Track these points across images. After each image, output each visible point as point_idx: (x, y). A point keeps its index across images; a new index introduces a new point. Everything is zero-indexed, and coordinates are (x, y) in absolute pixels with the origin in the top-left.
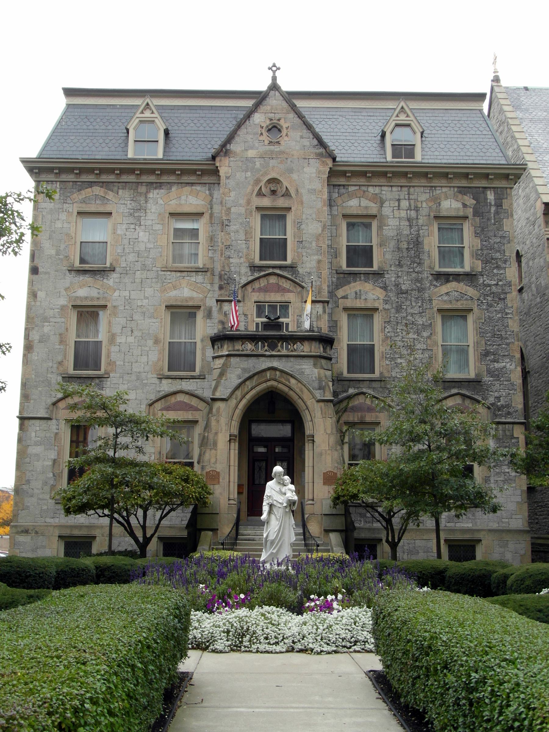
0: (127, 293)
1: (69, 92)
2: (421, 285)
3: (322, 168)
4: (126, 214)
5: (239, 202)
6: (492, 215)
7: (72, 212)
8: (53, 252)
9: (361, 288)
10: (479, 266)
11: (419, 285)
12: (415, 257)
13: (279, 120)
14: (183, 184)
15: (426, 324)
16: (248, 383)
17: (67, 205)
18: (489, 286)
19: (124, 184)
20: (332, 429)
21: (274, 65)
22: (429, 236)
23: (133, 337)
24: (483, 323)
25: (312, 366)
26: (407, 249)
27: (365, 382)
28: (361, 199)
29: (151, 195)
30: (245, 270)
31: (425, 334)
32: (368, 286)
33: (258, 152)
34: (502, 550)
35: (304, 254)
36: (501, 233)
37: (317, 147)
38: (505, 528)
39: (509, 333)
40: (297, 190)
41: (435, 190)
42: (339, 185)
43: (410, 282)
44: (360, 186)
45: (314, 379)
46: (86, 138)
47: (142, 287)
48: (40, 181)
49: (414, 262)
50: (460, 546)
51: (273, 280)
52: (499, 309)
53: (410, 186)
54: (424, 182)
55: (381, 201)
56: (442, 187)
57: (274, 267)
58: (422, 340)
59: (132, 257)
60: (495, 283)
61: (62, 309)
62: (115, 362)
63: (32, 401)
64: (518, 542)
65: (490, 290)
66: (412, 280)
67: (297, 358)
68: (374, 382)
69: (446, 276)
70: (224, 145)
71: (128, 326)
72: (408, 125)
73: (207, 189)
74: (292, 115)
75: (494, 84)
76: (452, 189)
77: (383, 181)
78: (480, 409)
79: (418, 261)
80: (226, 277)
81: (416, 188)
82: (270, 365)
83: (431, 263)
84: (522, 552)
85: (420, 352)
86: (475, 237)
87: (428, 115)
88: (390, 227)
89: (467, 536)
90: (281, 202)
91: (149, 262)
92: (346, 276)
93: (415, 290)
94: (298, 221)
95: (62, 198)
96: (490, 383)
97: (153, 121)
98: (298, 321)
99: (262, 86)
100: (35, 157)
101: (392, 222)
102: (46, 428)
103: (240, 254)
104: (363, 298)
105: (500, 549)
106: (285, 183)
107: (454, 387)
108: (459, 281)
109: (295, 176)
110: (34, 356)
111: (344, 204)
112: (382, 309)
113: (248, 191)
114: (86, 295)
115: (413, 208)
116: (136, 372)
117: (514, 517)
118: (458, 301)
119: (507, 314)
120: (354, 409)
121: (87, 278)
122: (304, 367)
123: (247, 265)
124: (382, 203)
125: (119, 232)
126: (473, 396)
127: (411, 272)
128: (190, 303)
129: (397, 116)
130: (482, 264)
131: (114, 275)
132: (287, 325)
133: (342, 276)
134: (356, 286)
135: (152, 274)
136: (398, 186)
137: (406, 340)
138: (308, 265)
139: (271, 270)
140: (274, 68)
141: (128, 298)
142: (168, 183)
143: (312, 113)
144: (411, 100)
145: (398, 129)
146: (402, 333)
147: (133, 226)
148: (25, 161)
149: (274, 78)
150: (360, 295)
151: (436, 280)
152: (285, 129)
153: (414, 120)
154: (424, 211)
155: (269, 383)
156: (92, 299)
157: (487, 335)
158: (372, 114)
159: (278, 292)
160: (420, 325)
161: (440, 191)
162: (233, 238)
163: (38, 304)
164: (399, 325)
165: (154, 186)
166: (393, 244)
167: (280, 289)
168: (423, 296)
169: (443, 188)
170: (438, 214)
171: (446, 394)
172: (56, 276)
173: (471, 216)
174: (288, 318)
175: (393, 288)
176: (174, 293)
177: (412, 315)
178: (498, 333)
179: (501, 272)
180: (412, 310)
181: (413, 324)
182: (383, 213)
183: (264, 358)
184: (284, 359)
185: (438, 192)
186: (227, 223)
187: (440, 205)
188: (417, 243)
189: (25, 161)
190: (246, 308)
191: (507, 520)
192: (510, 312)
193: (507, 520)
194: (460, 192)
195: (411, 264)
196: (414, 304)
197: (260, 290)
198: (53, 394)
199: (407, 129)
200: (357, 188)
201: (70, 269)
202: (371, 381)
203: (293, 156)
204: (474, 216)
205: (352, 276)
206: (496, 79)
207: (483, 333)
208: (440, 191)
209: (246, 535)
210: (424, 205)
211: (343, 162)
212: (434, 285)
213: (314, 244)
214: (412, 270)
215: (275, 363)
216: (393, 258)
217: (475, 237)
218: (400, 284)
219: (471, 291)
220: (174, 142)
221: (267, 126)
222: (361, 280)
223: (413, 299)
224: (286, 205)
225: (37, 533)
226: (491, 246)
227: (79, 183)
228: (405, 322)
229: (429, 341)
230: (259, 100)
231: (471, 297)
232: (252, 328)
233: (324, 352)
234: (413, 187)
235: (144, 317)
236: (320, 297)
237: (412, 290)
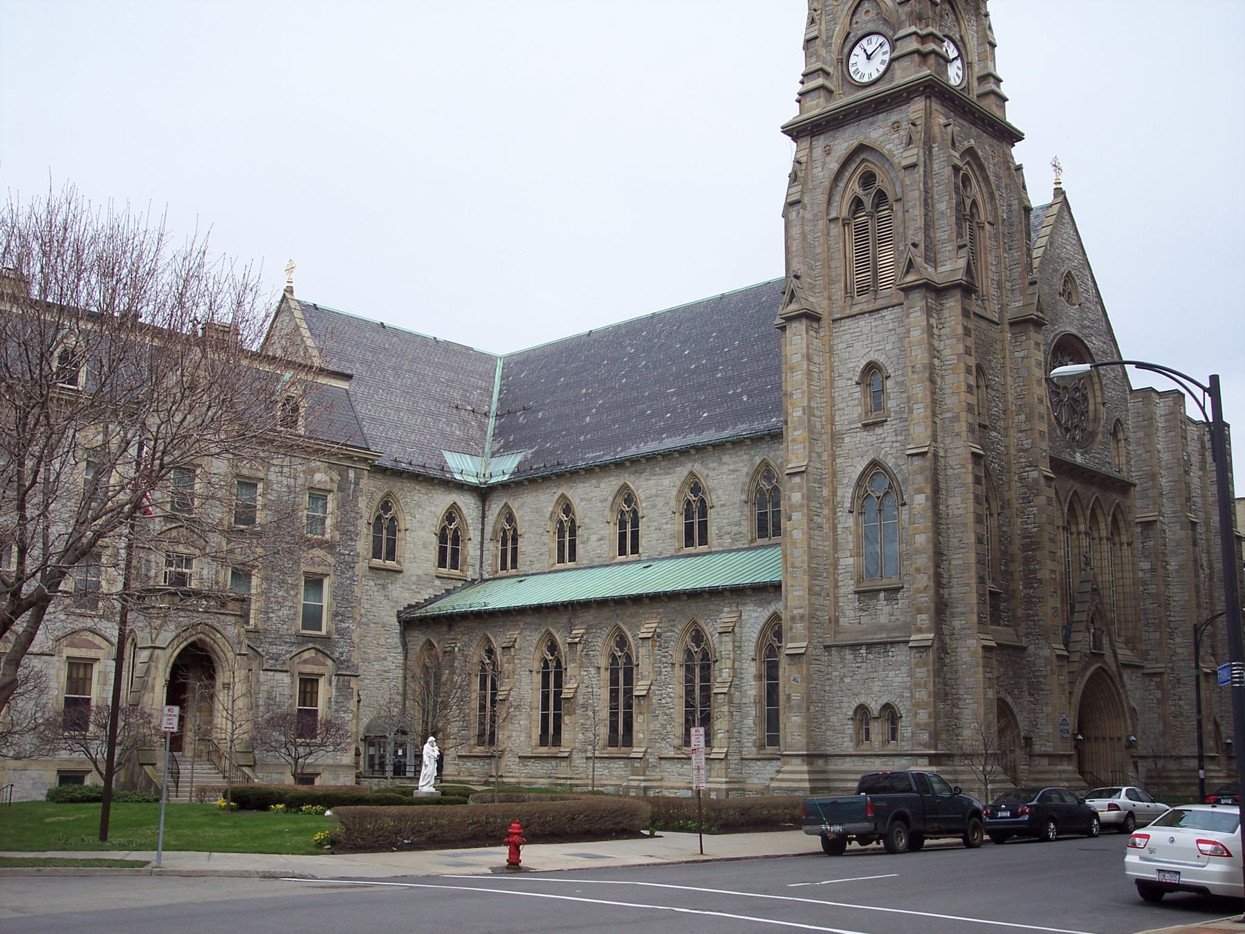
18: (344, 555)
85: (287, 608)
107: (310, 642)
119: (354, 581)
155: (201, 636)
179: (354, 543)
194: (329, 467)
206: (290, 290)
219: (330, 559)
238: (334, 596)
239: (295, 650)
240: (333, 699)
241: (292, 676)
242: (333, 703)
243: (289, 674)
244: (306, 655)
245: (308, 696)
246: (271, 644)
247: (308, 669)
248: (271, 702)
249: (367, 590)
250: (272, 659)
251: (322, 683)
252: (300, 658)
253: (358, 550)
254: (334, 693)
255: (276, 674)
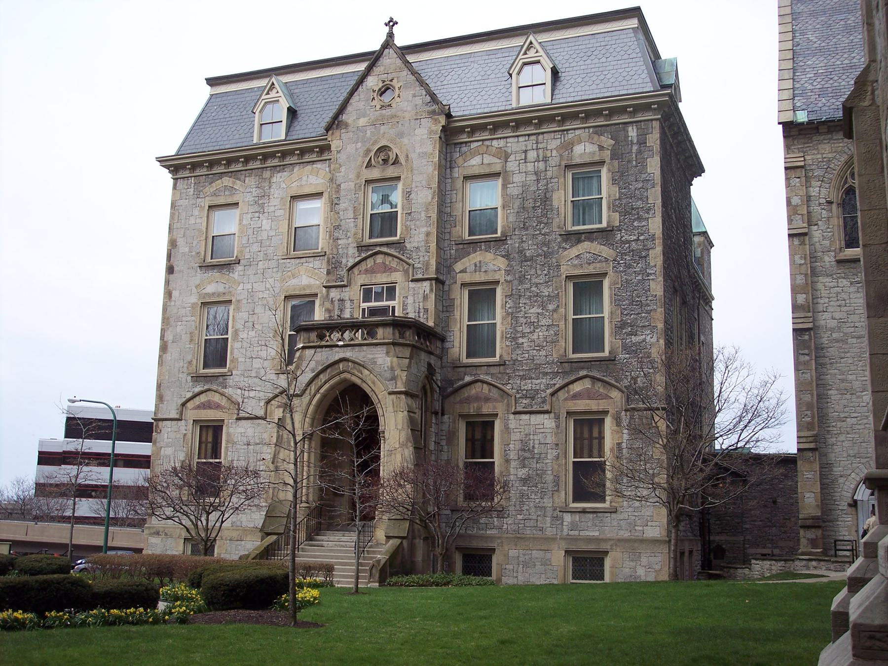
0: (249, 286)
1: (212, 82)
2: (549, 248)
3: (434, 128)
4: (252, 203)
5: (350, 177)
6: (634, 156)
7: (204, 207)
8: (187, 249)
9: (481, 259)
10: (616, 219)
11: (545, 249)
12: (542, 216)
13: (391, 81)
14: (304, 164)
15: (552, 294)
16: (321, 376)
17: (200, 200)
18: (629, 242)
19: (250, 172)
20: (403, 425)
21: (391, 20)
22: (558, 190)
23: (254, 332)
24: (619, 289)
25: (384, 355)
26: (533, 207)
27: (483, 368)
28: (485, 155)
29: (274, 180)
30: (352, 251)
31: (551, 307)
32: (489, 256)
33: (369, 119)
34: (633, 564)
35: (413, 227)
36: (643, 176)
37: (429, 104)
38: (638, 538)
39: (650, 298)
40: (407, 156)
41: (567, 134)
42: (462, 143)
43: (536, 247)
44: (483, 140)
45: (386, 369)
46: (599, 74)
47: (263, 279)
48: (177, 179)
49: (541, 223)
50: (585, 559)
51: (379, 259)
52: (639, 270)
53: (539, 134)
54: (554, 127)
55: (505, 155)
56: (575, 129)
57: (381, 245)
58: (547, 314)
59: (255, 247)
60: (635, 238)
61: (192, 307)
62: (237, 359)
63: (165, 402)
64: (652, 555)
65: (629, 247)
66: (537, 244)
67: (370, 347)
68: (492, 368)
69: (577, 236)
70: (336, 117)
71: (250, 320)
72: (538, 62)
73: (327, 166)
74: (405, 72)
75: (389, 38)
76: (587, 130)
77: (508, 133)
78: (615, 394)
79: (545, 221)
80: (334, 260)
81: (545, 135)
82: (342, 355)
83: (560, 222)
84: (657, 567)
85: (544, 328)
86: (613, 184)
87: (570, 45)
88: (515, 185)
89: (592, 547)
90: (391, 172)
91: (270, 251)
92: (465, 246)
93: (541, 256)
94: (408, 190)
95: (195, 193)
96: (625, 361)
97: (278, 101)
98: (404, 303)
99: (375, 45)
100: (173, 154)
101: (517, 178)
102: (176, 430)
103: (349, 234)
104: (483, 270)
105: (631, 563)
106: (396, 150)
107: (583, 368)
108: (591, 240)
109: (405, 141)
110: (168, 357)
111: (465, 164)
112: (503, 281)
113: (358, 164)
114: (213, 291)
115: (541, 159)
116: (256, 368)
117: (649, 524)
118: (590, 264)
119: (648, 275)
120: (468, 400)
121: (215, 274)
122: (377, 356)
123: (355, 245)
124: (506, 157)
125: (245, 222)
126: (605, 378)
127: (537, 235)
128: (308, 292)
129: (525, 53)
130: (620, 216)
131: (239, 268)
132: (394, 308)
133: (461, 246)
134: (476, 257)
135: (273, 264)
136: (525, 135)
137: (530, 315)
138: (416, 239)
139: (378, 249)
140: (391, 23)
141: (250, 290)
142: (291, 164)
143: (443, 64)
144: (541, 32)
145: (527, 69)
146: (525, 308)
147: (257, 215)
148: (164, 161)
149: (391, 35)
150: (480, 267)
151: (565, 241)
152: (397, 89)
153: (544, 55)
154: (553, 162)
155: (343, 376)
156: (219, 295)
157: (624, 303)
158: (507, 54)
159: (384, 272)
160: (545, 296)
161: (573, 135)
162: (342, 218)
163: (173, 303)
164: (522, 299)
165: (278, 169)
166: (517, 203)
167: (387, 269)
168: (550, 262)
169: (576, 131)
170: (570, 163)
171: (573, 378)
172: (189, 273)
173: (608, 160)
174: (395, 300)
175: (516, 255)
176: (293, 282)
177: (537, 285)
178: (637, 299)
179: (644, 223)
180: (536, 280)
181: (537, 296)
182: (508, 169)
183: (337, 349)
184: (357, 348)
185: (570, 136)
186: (336, 202)
187: (572, 151)
188: (545, 200)
189: (164, 161)
190: (352, 293)
191: (641, 528)
192: (652, 272)
193: (641, 528)
194: (596, 133)
195: (537, 225)
196: (539, 272)
197: (367, 271)
198: (183, 394)
199: (538, 66)
200: (480, 143)
201: (200, 265)
202: (489, 365)
203: (404, 118)
204: (612, 159)
205: (471, 245)
207: (619, 300)
208: (573, 135)
209: (319, 541)
210: (554, 153)
211: (459, 116)
212: (563, 248)
213: (423, 214)
214: (538, 232)
215: (348, 353)
216: (518, 220)
217: (613, 184)
218: (525, 249)
219: (606, 251)
220: (300, 119)
221: (380, 89)
222: (481, 250)
223: (538, 266)
224: (396, 175)
225: (166, 534)
226: (632, 194)
227: (210, 176)
228: (529, 294)
229: (555, 316)
230: (371, 61)
231: (605, 258)
232: (359, 316)
233: (400, 338)
234: (543, 133)
235: (265, 310)
236: (428, 274)
237: (537, 256)
238: (617, 301)
239: (559, 382)
240: (624, 445)
241: (557, 417)
242: (625, 451)
243: (552, 415)
244: (577, 387)
245: (595, 442)
246: (523, 378)
247: (581, 405)
248: (527, 455)
249: (837, 293)
250: (526, 397)
251: (608, 422)
252: (568, 392)
253: (651, 231)
254: (626, 437)
255: (533, 417)
